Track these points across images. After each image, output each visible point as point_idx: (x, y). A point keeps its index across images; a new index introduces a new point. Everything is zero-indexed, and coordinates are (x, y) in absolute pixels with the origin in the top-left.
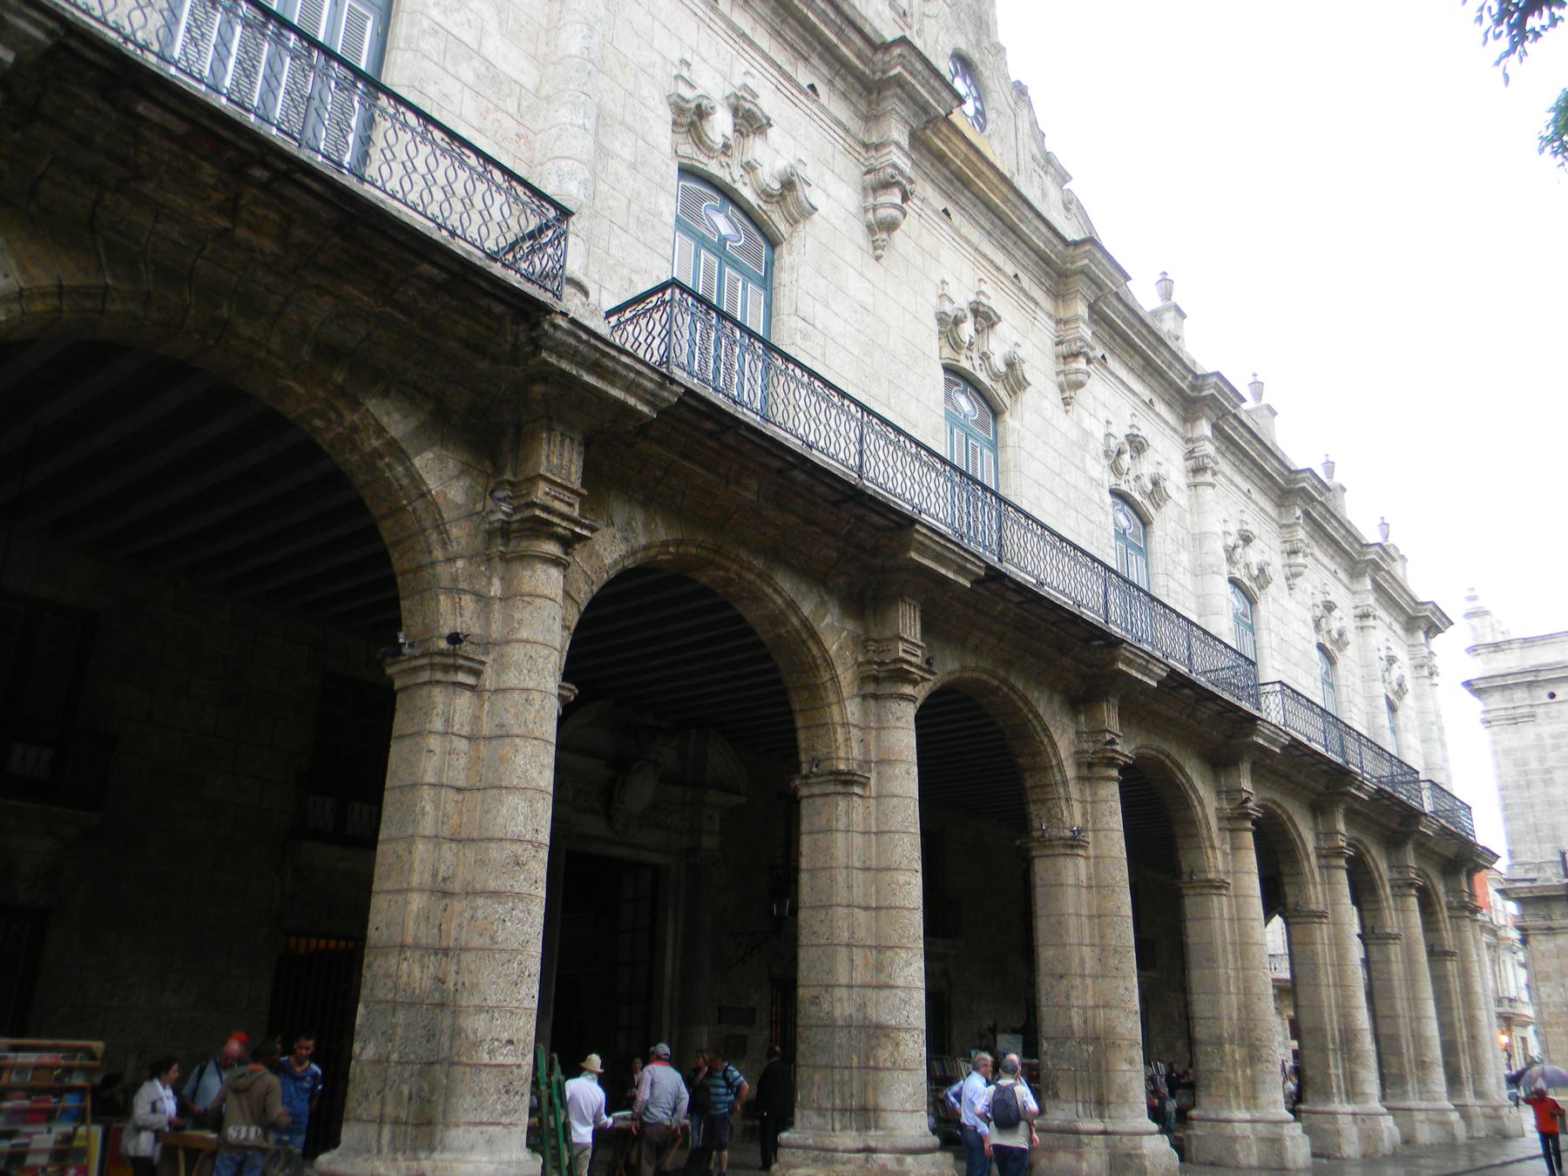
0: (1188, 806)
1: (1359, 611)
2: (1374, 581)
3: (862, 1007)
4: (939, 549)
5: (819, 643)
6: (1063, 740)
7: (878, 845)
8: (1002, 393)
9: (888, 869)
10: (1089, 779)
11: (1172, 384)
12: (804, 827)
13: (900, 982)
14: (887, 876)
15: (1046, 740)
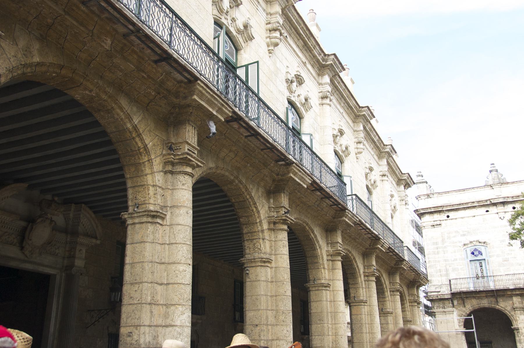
0: (315, 249)
1: (381, 173)
2: (387, 162)
3: (155, 337)
4: (209, 97)
5: (142, 140)
6: (263, 210)
7: (169, 251)
8: (241, 40)
9: (174, 263)
10: (274, 230)
11: (315, 56)
12: (129, 241)
13: (178, 323)
14: (173, 267)
15: (255, 209)
